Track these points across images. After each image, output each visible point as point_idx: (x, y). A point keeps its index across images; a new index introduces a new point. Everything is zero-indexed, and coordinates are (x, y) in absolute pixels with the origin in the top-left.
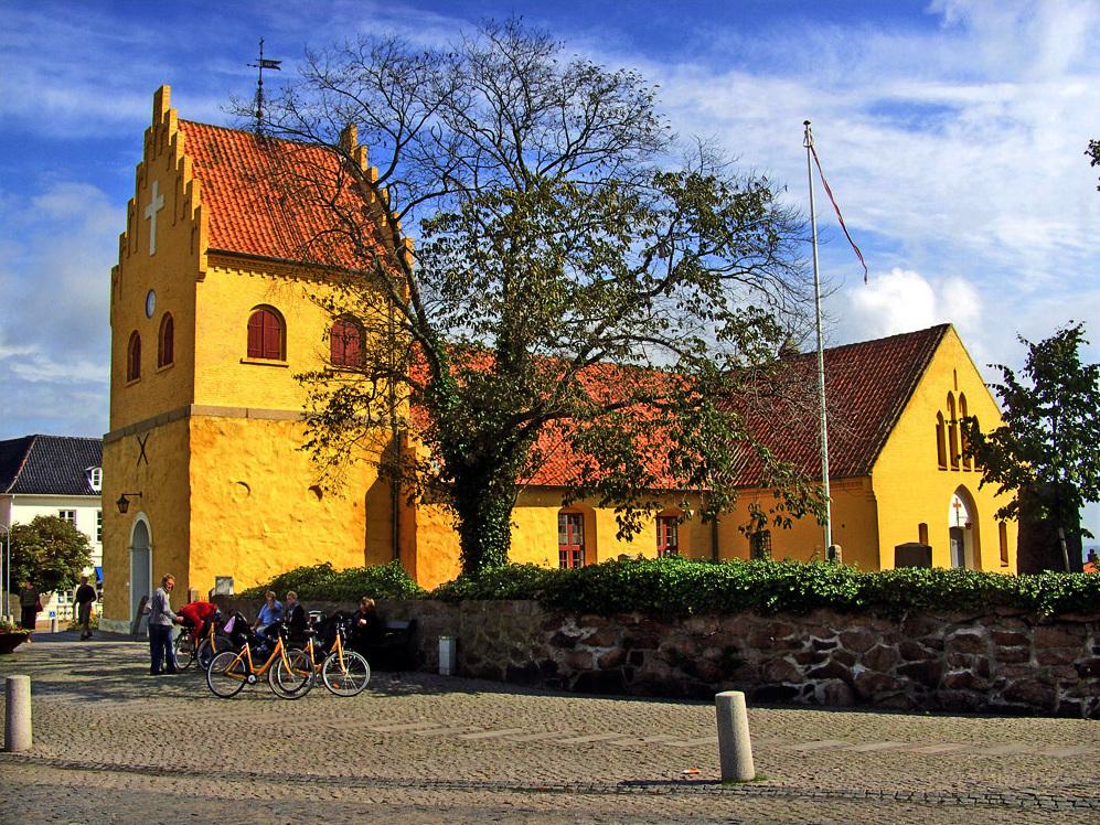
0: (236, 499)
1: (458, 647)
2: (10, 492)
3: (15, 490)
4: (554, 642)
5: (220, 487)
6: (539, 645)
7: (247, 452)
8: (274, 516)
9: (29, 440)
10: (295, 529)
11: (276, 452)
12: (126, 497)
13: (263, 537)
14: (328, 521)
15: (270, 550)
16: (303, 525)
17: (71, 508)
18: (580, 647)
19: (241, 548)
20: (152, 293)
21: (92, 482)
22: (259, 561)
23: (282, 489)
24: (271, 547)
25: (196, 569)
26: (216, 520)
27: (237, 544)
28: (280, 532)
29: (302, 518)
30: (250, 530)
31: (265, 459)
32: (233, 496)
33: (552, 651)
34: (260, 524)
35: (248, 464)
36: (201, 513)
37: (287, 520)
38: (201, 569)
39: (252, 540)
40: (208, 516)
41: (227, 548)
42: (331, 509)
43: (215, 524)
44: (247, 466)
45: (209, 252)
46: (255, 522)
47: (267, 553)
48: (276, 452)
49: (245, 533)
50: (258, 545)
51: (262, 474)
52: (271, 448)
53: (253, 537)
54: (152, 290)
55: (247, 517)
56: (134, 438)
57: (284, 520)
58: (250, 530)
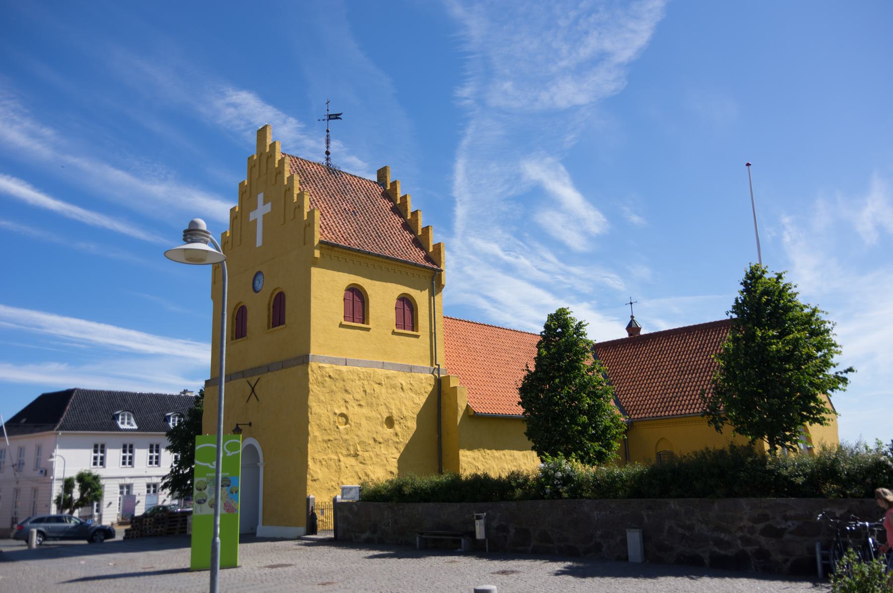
0: (339, 427)
1: (645, 539)
2: (57, 430)
3: (61, 428)
4: (764, 532)
5: (329, 417)
6: (748, 535)
7: (346, 391)
8: (363, 439)
9: (67, 395)
10: (377, 450)
11: (365, 391)
12: (239, 426)
13: (356, 455)
14: (397, 443)
15: (361, 465)
16: (382, 445)
17: (131, 442)
18: (787, 536)
19: (342, 464)
20: (260, 277)
21: (119, 423)
22: (354, 474)
23: (368, 418)
24: (361, 463)
25: (312, 481)
26: (326, 442)
27: (339, 461)
28: (367, 451)
29: (381, 440)
30: (348, 450)
31: (358, 396)
32: (337, 424)
33: (763, 540)
34: (355, 446)
35: (347, 400)
36: (315, 437)
37: (371, 442)
38: (315, 480)
39: (349, 457)
40: (321, 440)
41: (332, 463)
42: (400, 434)
43: (325, 445)
44: (346, 402)
45: (321, 242)
46: (351, 443)
47: (359, 468)
48: (365, 391)
49: (345, 452)
50: (352, 461)
51: (356, 407)
52: (362, 389)
53: (349, 455)
54: (259, 273)
55: (346, 440)
56: (243, 381)
57: (370, 442)
58: (348, 450)
